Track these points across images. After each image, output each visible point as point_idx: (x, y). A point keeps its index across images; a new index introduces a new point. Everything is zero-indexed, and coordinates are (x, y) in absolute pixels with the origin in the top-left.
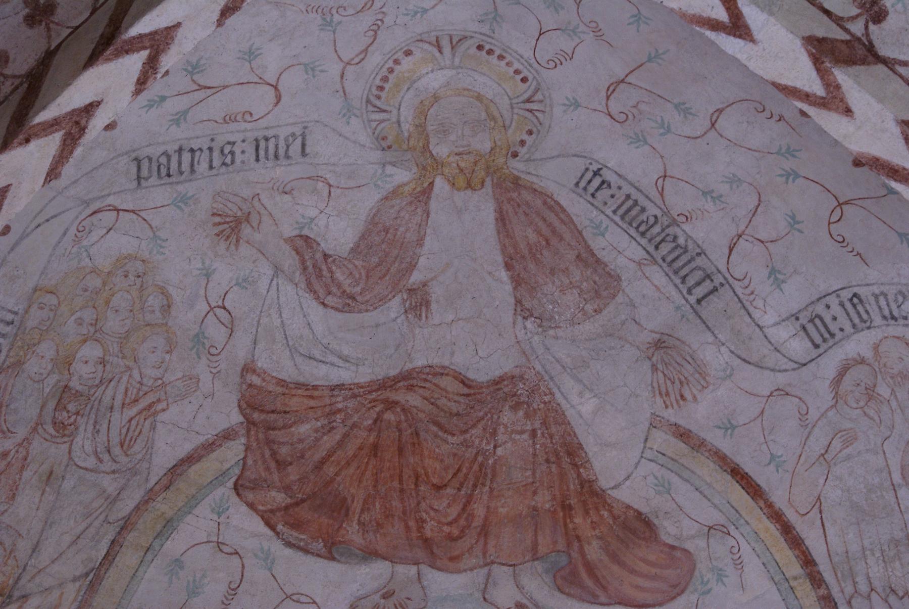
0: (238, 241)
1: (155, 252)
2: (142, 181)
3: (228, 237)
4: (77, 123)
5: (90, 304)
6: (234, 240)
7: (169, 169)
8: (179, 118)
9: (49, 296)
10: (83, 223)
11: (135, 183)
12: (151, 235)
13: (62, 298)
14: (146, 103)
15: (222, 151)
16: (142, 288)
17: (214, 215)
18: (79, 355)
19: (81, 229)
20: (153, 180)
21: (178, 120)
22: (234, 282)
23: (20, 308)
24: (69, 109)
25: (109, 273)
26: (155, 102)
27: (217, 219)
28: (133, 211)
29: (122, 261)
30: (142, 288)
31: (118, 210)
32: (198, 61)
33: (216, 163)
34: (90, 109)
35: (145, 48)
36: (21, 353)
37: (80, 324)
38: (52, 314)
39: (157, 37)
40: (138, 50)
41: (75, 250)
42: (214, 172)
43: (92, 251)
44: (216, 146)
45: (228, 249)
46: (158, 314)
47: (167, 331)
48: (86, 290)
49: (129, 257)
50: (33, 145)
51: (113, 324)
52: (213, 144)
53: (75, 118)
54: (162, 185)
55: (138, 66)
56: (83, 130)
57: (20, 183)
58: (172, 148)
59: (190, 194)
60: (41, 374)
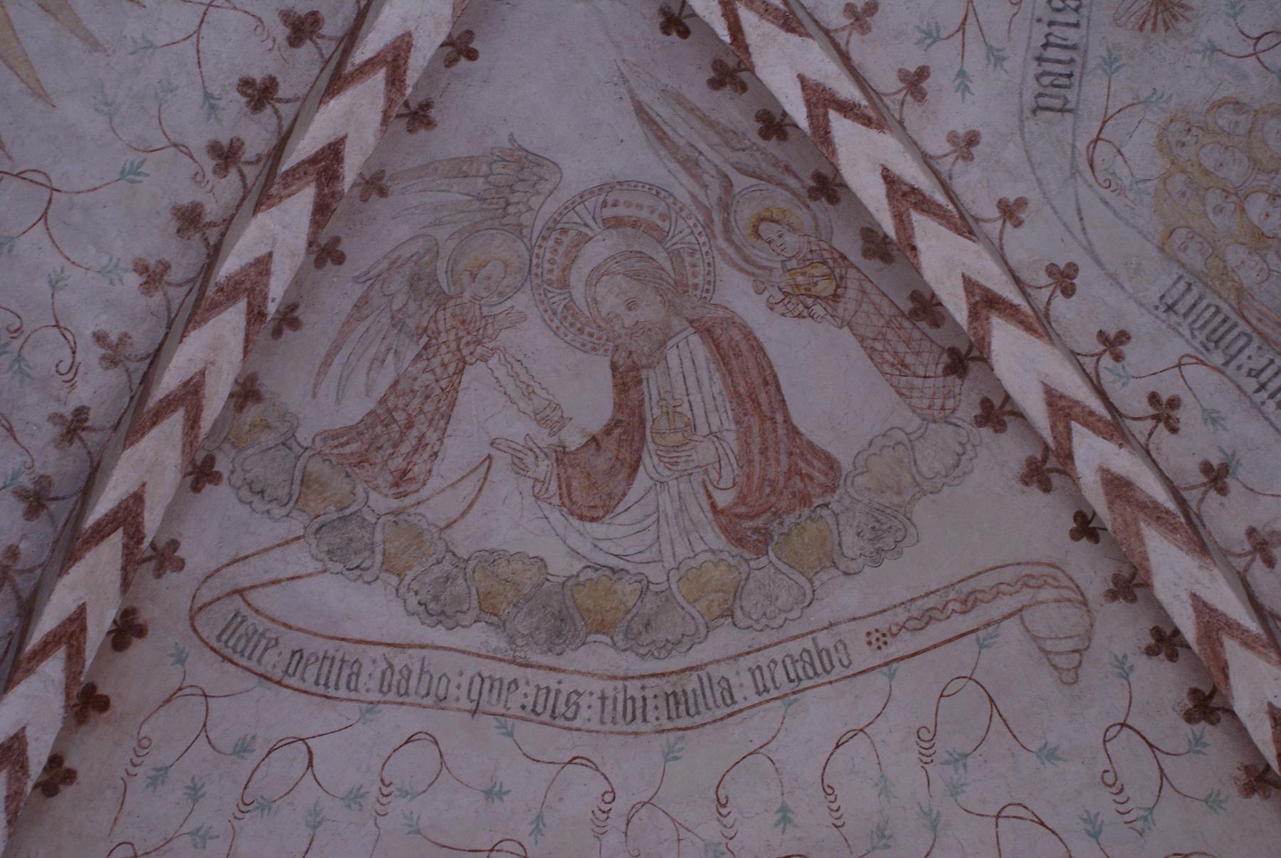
0: (1182, 6)
1: (1164, 105)
2: (1068, 107)
3: (1174, 17)
4: (904, 195)
5: (1201, 193)
6: (1181, 10)
7: (1061, 75)
8: (996, 57)
9: (1174, 236)
10: (1101, 180)
11: (1067, 115)
12: (1142, 106)
13: (1182, 222)
14: (959, 95)
15: (1059, 10)
16: (1204, 129)
17: (1141, 29)
18: (1256, 222)
19: (1107, 184)
20: (1071, 95)
21: (997, 58)
22: (1231, 21)
23: (1176, 271)
24: (885, 202)
25: (1173, 163)
26: (962, 83)
27: (1149, 26)
28: (1104, 122)
29: (1163, 145)
30: (1204, 129)
31: (1098, 139)
32: (921, 31)
33: (1072, 18)
34: (890, 179)
35: (826, 114)
36: (1229, 284)
37: (1222, 210)
38: (1197, 239)
39: (814, 99)
40: (827, 121)
41: (1131, 195)
42: (1084, 22)
43: (1139, 175)
44: (1048, 15)
45: (1188, 20)
46: (1242, 118)
47: (1264, 113)
48: (1184, 194)
49: (1161, 137)
50: (921, 244)
51: (1234, 172)
52: (1046, 20)
53: (898, 196)
54: (1080, 86)
55: (848, 123)
56: (914, 190)
57: (964, 264)
58: (1033, 68)
59: (1105, 54)
60: (1262, 269)
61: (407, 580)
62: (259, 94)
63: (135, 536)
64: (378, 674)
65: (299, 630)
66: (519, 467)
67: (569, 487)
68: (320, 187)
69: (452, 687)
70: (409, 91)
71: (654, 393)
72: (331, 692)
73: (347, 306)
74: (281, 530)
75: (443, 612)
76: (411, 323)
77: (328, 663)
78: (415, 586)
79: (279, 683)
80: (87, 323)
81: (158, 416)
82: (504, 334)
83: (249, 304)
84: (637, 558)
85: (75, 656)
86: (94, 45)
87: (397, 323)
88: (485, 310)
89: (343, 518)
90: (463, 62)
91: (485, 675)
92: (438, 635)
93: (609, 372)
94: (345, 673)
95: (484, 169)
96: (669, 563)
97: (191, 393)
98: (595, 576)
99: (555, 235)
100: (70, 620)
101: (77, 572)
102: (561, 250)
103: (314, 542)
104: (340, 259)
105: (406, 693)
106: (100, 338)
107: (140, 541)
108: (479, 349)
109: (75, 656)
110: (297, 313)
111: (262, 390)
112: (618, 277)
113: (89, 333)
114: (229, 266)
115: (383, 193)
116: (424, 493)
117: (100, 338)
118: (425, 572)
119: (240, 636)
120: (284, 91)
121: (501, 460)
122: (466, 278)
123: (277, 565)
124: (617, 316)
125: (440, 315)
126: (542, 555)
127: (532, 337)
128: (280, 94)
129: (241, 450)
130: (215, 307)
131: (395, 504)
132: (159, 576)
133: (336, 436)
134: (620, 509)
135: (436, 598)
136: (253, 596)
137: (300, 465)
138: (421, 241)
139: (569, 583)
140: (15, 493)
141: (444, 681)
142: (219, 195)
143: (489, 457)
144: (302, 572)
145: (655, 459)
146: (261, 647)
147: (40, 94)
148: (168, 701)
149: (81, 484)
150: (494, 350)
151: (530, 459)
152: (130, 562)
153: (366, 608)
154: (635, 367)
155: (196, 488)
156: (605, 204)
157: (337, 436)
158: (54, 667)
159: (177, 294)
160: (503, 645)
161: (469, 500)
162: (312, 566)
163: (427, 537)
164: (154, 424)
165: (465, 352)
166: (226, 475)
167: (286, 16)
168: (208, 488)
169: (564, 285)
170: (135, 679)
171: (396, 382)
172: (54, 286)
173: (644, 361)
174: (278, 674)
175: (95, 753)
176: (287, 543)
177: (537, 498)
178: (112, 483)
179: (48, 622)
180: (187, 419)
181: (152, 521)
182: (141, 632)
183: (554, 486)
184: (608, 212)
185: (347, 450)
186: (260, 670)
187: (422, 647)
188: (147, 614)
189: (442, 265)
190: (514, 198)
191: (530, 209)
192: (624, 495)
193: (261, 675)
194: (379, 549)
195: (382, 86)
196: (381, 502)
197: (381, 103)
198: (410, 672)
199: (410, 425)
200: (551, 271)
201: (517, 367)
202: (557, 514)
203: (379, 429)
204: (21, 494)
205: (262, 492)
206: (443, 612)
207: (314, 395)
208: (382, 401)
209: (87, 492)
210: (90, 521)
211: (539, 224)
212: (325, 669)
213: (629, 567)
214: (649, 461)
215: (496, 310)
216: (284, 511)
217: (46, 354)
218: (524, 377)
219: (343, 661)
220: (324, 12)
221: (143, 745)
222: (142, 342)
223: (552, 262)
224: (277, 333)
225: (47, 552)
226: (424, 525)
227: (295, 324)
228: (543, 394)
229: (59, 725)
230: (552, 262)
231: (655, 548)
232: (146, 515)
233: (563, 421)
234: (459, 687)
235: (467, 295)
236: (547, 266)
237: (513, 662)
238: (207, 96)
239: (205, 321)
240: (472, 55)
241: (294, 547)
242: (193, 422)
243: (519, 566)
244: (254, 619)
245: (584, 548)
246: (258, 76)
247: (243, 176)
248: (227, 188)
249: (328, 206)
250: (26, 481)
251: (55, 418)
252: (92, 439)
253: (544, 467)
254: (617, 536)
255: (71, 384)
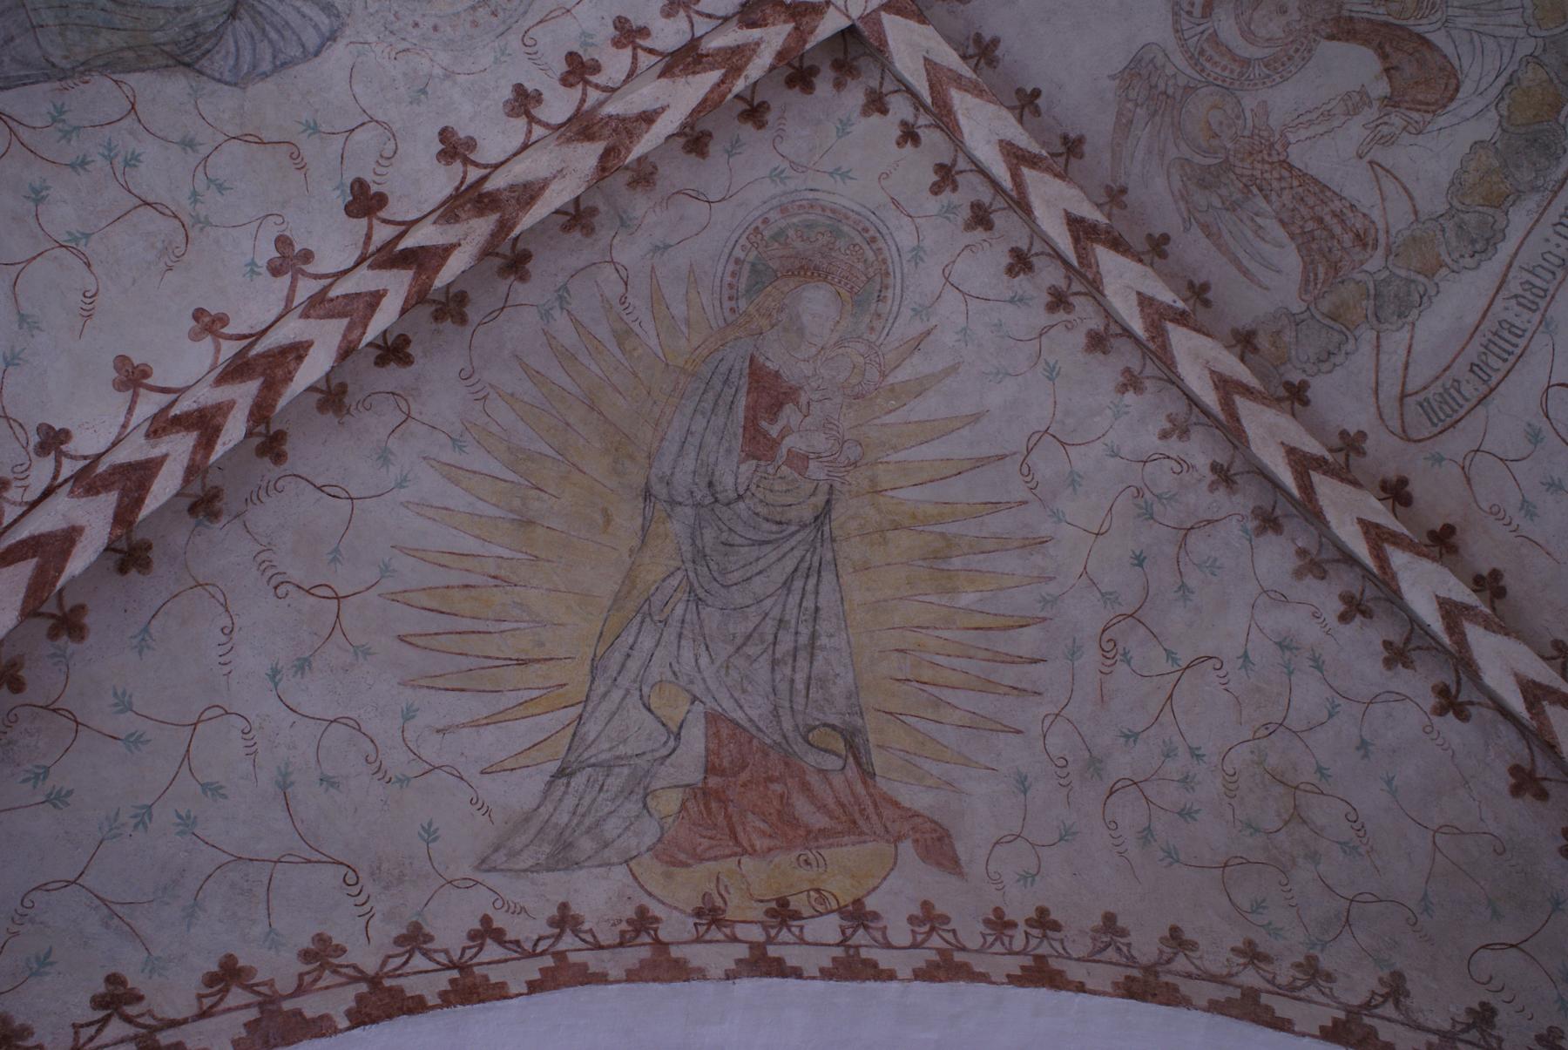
61: (1448, 260)
62: (1020, 263)
63: (1320, 464)
64: (1518, 309)
65: (1454, 360)
66: (1388, 141)
67: (1420, 103)
68: (1098, 241)
69: (1556, 251)
70: (1044, 153)
71: (1365, 8)
72: (1518, 351)
73: (1204, 242)
74: (1366, 349)
75: (1488, 240)
76: (1237, 196)
77: (1491, 346)
78: (1456, 255)
79: (1492, 390)
80: (1150, 440)
81: (1234, 416)
82: (1272, 122)
83: (1171, 321)
84: (1506, 60)
85: (1396, 540)
86: (953, 369)
87: (1233, 207)
88: (1247, 133)
89: (1376, 296)
90: (1040, 102)
91: (1557, 220)
92: (1506, 249)
93: (1335, 43)
94: (1506, 334)
95: (1130, 105)
96: (1521, 32)
97: (1225, 386)
98: (1507, 101)
99: (1202, 60)
100: (1366, 533)
101: (1331, 516)
102: (1217, 58)
103: (1386, 326)
104: (1166, 238)
105: (1545, 291)
106: (1164, 435)
107: (1326, 461)
108: (1278, 147)
109: (1396, 540)
110: (1197, 283)
111: (1248, 328)
112: (1256, 16)
113: (1158, 442)
114: (1137, 326)
115: (1123, 191)
116: (1381, 225)
117: (1164, 435)
118: (1447, 243)
119: (1439, 409)
120: (1023, 245)
121: (1379, 154)
122: (1215, 142)
123: (1393, 359)
124: (1288, 24)
125: (1238, 171)
126: (1471, 142)
127: (1282, 100)
128: (1025, 248)
129: (1289, 359)
130: (1165, 347)
131: (1381, 251)
132: (1364, 454)
133: (1306, 281)
134: (1456, 63)
135: (1473, 242)
136: (1410, 388)
137: (1318, 317)
138: (1173, 170)
139: (1505, 124)
140: (1257, 535)
141: (1547, 256)
142: (1086, 316)
143: (1371, 162)
144: (1407, 342)
145: (1424, 21)
146: (1455, 394)
147: (976, 418)
148: (1469, 480)
149: (1269, 486)
150: (1282, 134)
151: (1385, 129)
152: (1343, 474)
153: (1459, 300)
154: (1337, 20)
155: (1306, 403)
156: (1189, 13)
157: (1307, 282)
158: (1399, 558)
159: (1151, 369)
160: (1537, 197)
161: (1401, 190)
162: (1405, 334)
163: (1418, 233)
164: (1238, 420)
165: (1275, 158)
166: (1304, 377)
167: (969, 227)
168: (1309, 394)
169: (1246, 63)
170: (1438, 498)
171: (1281, 221)
172: (1115, 454)
173: (1334, 10)
174: (1484, 389)
175: (1484, 551)
176: (1378, 346)
177: (1420, 132)
178: (1272, 467)
179: (1361, 549)
180: (1243, 395)
181: (1312, 446)
182: (1403, 482)
183: (1416, 115)
184: (1197, 12)
185: (1321, 276)
186: (1474, 401)
187: (1510, 266)
188: (1391, 472)
189: (1197, 159)
190: (1162, 86)
191: (1174, 76)
192: (1445, 57)
193: (1479, 402)
194: (1413, 276)
195: (1034, 173)
196: (1375, 262)
197: (1048, 177)
198: (1528, 282)
199: (1320, 220)
200: (1232, 71)
201: (1301, 119)
202: (1441, 119)
203: (1314, 246)
204: (1260, 531)
205: (1330, 353)
206: (1488, 240)
207: (1267, 289)
208: (1292, 237)
209: (1276, 485)
210: (1295, 492)
211: (1189, 71)
212: (1496, 350)
213: (1510, 70)
214: (1423, 28)
215: (1250, 123)
216: (1352, 341)
217: (1163, 477)
218: (1314, 115)
219: (1495, 334)
220: (973, 199)
221: (1496, 512)
222: (1179, 407)
223: (1224, 68)
224: (1207, 303)
225: (1312, 529)
226: (1407, 233)
227: (1205, 287)
228: (1333, 103)
229: (1446, 571)
230: (1224, 68)
231: (1502, 41)
232: (1306, 449)
233: (1363, 93)
234: (1558, 246)
235: (1229, 145)
236: (1226, 73)
237: (1555, 193)
238: (1012, 301)
239: (1173, 357)
240: (1036, 93)
241: (1383, 342)
242: (1247, 391)
243: (1473, 164)
244: (1429, 394)
245: (1479, 103)
246: (1006, 260)
247: (1076, 294)
248: (1083, 307)
249: (1115, 238)
250: (1252, 524)
251: (1212, 487)
252: (1238, 466)
253: (1397, 120)
254: (1480, 72)
255: (1191, 467)
